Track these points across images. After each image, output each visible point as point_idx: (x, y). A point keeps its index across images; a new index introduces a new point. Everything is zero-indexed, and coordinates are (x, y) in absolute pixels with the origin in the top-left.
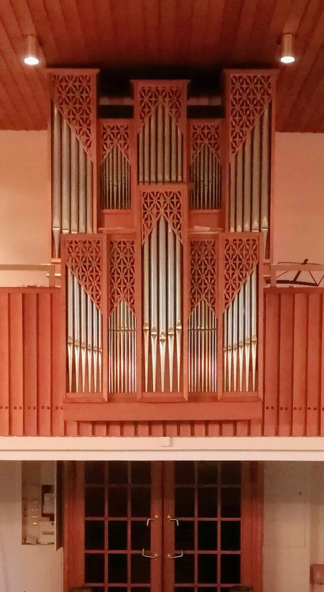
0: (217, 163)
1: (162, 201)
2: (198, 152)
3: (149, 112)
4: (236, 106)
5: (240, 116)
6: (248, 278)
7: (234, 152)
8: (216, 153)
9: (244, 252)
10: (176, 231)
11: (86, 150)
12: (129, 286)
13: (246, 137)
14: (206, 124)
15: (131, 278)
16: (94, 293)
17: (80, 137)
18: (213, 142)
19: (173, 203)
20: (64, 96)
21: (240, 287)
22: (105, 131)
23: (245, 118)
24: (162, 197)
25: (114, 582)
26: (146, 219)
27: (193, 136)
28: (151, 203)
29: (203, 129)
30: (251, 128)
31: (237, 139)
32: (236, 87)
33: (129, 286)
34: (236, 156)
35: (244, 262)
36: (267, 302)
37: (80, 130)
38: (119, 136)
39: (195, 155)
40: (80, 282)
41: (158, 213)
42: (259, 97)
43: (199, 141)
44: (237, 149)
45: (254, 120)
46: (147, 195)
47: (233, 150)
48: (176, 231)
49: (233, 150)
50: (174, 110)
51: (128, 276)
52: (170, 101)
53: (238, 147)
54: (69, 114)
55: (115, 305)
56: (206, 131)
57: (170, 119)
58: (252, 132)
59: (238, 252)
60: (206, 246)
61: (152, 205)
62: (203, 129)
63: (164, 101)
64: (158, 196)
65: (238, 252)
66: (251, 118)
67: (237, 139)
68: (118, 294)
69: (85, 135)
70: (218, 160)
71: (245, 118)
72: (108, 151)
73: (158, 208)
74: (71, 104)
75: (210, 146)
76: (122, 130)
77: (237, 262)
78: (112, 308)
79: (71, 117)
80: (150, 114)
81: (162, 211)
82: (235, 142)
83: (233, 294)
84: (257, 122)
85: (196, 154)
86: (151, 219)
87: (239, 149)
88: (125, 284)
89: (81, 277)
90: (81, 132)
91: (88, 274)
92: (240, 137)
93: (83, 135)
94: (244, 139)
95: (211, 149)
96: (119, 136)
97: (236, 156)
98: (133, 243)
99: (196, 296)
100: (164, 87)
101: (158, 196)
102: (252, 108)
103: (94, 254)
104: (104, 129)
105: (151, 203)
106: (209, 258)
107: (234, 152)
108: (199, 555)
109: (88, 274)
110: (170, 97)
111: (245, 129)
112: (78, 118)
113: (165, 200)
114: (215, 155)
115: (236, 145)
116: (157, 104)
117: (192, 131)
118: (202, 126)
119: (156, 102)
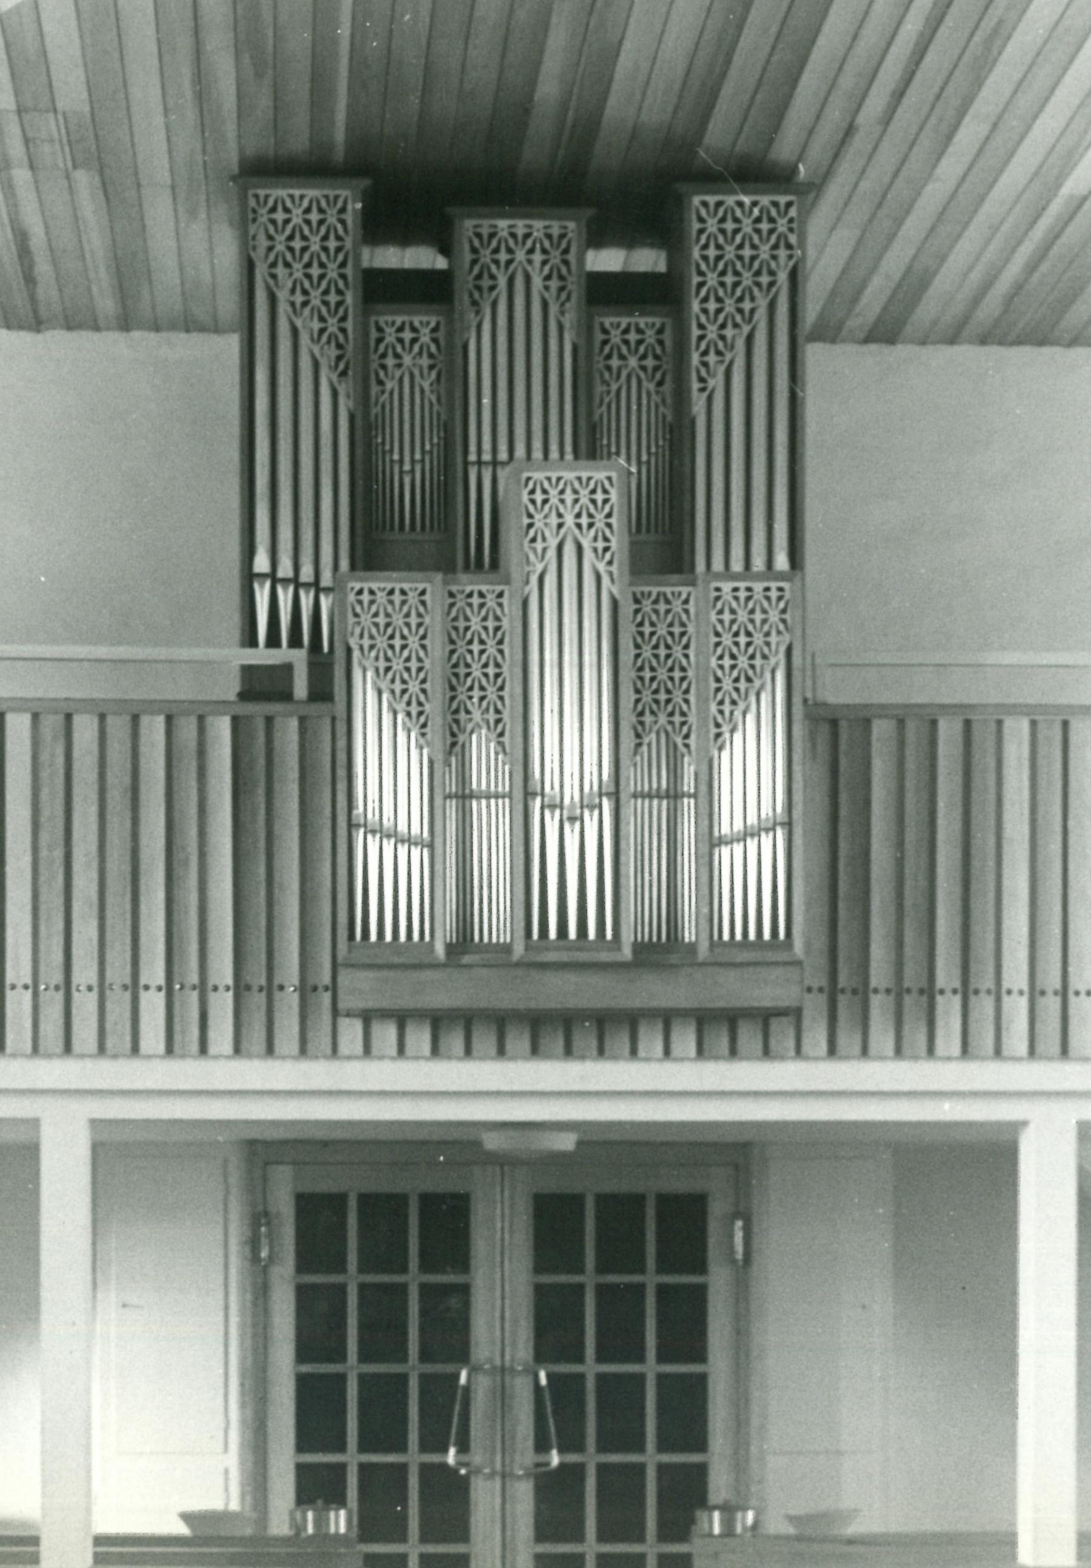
0: (660, 419)
1: (569, 497)
2: (614, 387)
3: (492, 288)
4: (488, 260)
5: (719, 300)
6: (768, 676)
7: (703, 390)
8: (657, 392)
9: (758, 617)
10: (601, 567)
11: (336, 384)
12: (491, 693)
13: (735, 351)
14: (633, 320)
15: (497, 676)
16: (414, 709)
17: (322, 348)
18: (650, 362)
19: (594, 502)
20: (280, 247)
21: (749, 699)
22: (435, 335)
23: (730, 306)
24: (569, 491)
25: (375, 1450)
26: (533, 540)
27: (602, 350)
28: (545, 501)
29: (626, 331)
30: (746, 329)
31: (712, 358)
32: (709, 230)
33: (491, 693)
34: (710, 399)
35: (758, 639)
36: (903, 662)
37: (322, 331)
38: (416, 348)
39: (605, 395)
40: (378, 682)
41: (560, 526)
42: (765, 251)
43: (615, 362)
44: (711, 382)
45: (752, 311)
46: (535, 484)
47: (702, 385)
48: (601, 567)
49: (702, 385)
50: (554, 284)
51: (491, 671)
52: (544, 263)
53: (714, 376)
54: (293, 291)
55: (461, 738)
56: (633, 337)
57: (545, 305)
58: (750, 340)
59: (742, 616)
60: (668, 602)
61: (547, 507)
62: (626, 331)
63: (530, 262)
64: (561, 486)
65: (742, 616)
66: (747, 305)
67: (712, 358)
68: (468, 712)
69: (333, 344)
70: (662, 409)
71: (730, 306)
72: (389, 385)
73: (560, 515)
74: (297, 266)
75: (642, 375)
76: (650, 333)
77: (742, 639)
78: (454, 744)
79: (299, 298)
80: (494, 293)
81: (569, 520)
82: (705, 364)
83: (732, 713)
84: (761, 315)
85: (609, 392)
86: (544, 539)
87: (716, 382)
88: (482, 688)
89: (382, 671)
90: (324, 338)
91: (398, 665)
92: (719, 353)
93: (329, 342)
94: (728, 357)
95: (645, 383)
96: (416, 348)
97: (710, 399)
98: (501, 595)
99: (648, 718)
100: (530, 227)
101: (561, 486)
102: (747, 278)
103: (414, 620)
104: (605, 331)
105: (545, 501)
106: (677, 630)
107: (703, 390)
108: (600, 1359)
109: (398, 665)
110: (544, 251)
111: (729, 332)
112: (316, 302)
113: (576, 496)
114: (654, 397)
115: (708, 372)
116: (512, 267)
117: (599, 337)
118: (623, 326)
119: (509, 262)
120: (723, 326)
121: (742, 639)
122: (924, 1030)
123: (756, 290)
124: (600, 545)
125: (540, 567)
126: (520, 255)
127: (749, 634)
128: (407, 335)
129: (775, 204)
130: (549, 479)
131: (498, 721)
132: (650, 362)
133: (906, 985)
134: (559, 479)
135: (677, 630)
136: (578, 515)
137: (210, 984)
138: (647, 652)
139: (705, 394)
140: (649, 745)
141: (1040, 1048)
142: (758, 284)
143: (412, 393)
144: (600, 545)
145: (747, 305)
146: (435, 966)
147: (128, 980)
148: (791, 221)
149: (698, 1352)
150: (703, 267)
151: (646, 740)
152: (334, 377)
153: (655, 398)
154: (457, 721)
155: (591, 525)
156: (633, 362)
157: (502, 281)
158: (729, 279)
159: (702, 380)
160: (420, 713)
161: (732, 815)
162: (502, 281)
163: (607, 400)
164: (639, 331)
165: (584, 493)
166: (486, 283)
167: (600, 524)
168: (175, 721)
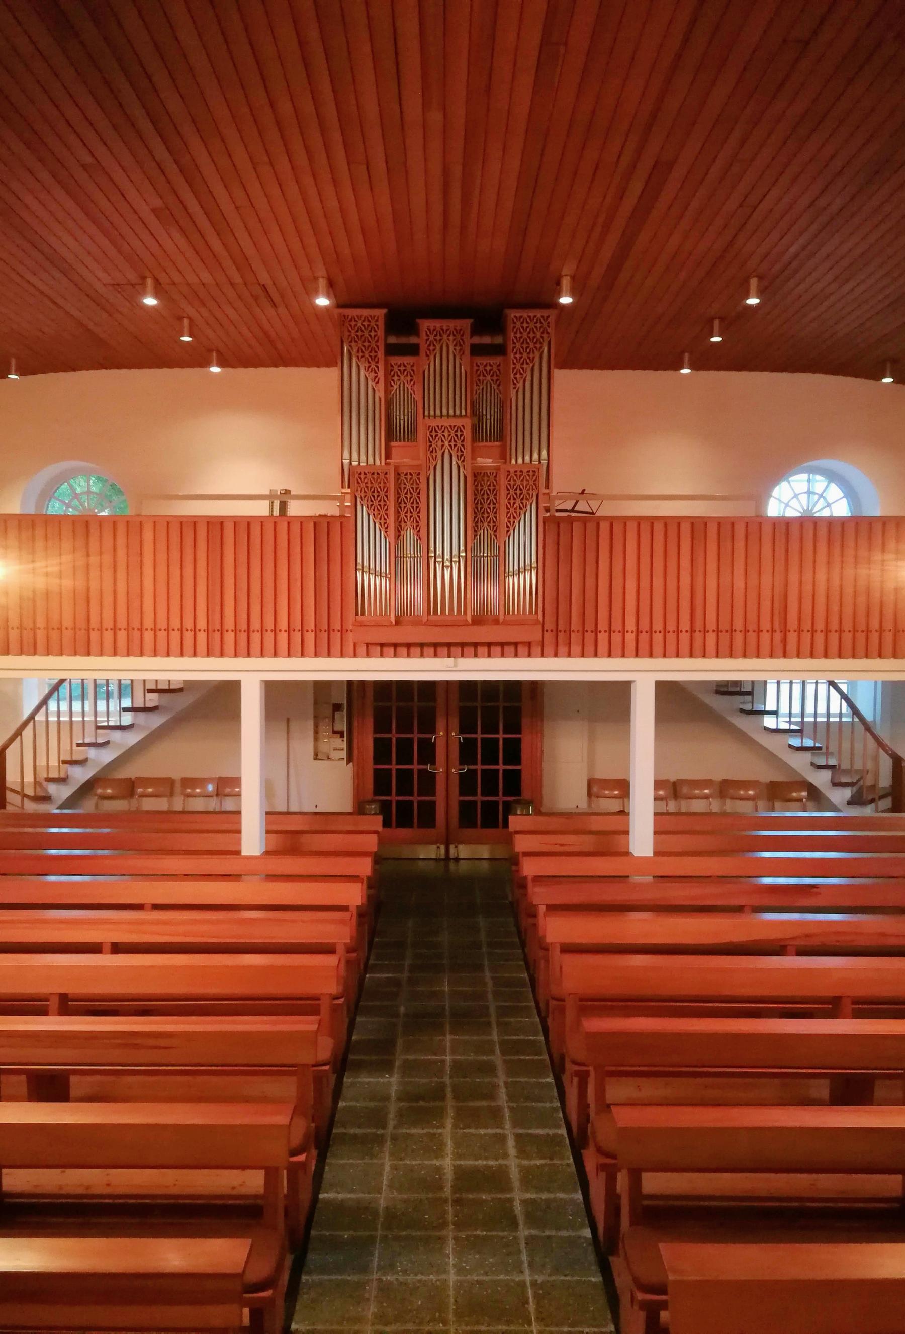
1: (446, 434)
3: (434, 350)
5: (521, 353)
7: (514, 388)
15: (417, 507)
16: (382, 521)
23: (525, 355)
28: (436, 436)
29: (486, 365)
30: (531, 365)
31: (518, 376)
34: (517, 392)
37: (369, 367)
38: (406, 373)
41: (443, 446)
44: (518, 385)
45: (534, 358)
48: (460, 462)
50: (458, 348)
51: (415, 505)
52: (454, 340)
55: (402, 533)
56: (488, 368)
59: (518, 482)
67: (518, 376)
71: (525, 355)
72: (395, 387)
77: (518, 492)
78: (399, 536)
82: (516, 378)
83: (514, 522)
84: (537, 360)
87: (520, 385)
88: (411, 513)
90: (370, 369)
91: (376, 503)
92: (521, 374)
94: (525, 375)
97: (517, 392)
102: (532, 346)
105: (436, 436)
109: (376, 503)
111: (525, 366)
114: (497, 391)
117: (476, 368)
119: (440, 340)
120: (523, 364)
121: (518, 492)
122: (540, 648)
123: (535, 349)
124: (459, 453)
125: (434, 463)
126: (445, 337)
127: (521, 490)
128: (402, 368)
129: (529, 317)
130: (438, 426)
131: (417, 526)
132: (495, 378)
133: (621, 634)
134: (442, 426)
135: (492, 488)
136: (450, 441)
137: (649, 633)
138: (479, 497)
139: (515, 390)
140: (480, 535)
141: (252, 652)
142: (536, 347)
143: (404, 390)
144: (459, 453)
145: (531, 356)
146: (468, 625)
147: (593, 629)
148: (549, 323)
149: (377, 773)
150: (515, 341)
151: (479, 534)
152: (374, 384)
153: (497, 391)
154: (400, 526)
155: (455, 445)
156: (489, 378)
157: (438, 348)
158: (525, 346)
159: (515, 384)
160: (385, 523)
161: (155, 579)
162: (438, 348)
163: (478, 392)
164: (491, 365)
165: (453, 432)
166: (432, 348)
167: (459, 444)
168: (291, 524)
